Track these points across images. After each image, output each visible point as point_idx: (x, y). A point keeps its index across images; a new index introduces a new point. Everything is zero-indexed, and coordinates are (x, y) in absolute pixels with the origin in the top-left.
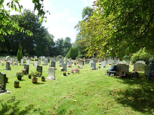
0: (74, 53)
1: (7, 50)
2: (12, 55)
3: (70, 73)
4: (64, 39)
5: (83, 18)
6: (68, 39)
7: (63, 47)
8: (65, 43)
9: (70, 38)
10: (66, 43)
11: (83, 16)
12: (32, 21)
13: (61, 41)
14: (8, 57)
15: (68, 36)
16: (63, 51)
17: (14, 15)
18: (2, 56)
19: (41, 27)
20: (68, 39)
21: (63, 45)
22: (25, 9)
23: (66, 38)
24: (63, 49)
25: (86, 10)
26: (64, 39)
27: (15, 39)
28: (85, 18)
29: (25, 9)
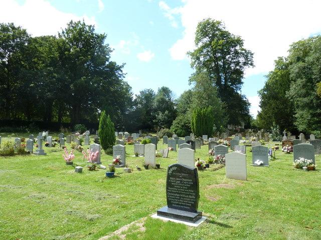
0: (206, 123)
1: (23, 116)
2: (37, 133)
3: (136, 169)
4: (156, 91)
5: (197, 44)
6: (165, 91)
7: (155, 110)
8: (158, 101)
9: (171, 88)
10: (162, 101)
11: (198, 40)
12: (211, 35)
13: (148, 96)
14: (44, 134)
15: (166, 86)
16: (155, 118)
17: (45, 36)
18: (2, 131)
19: (107, 63)
20: (165, 91)
21: (155, 104)
22: (72, 21)
23: (160, 88)
24: (156, 116)
25: (205, 27)
26: (156, 91)
27: (49, 91)
28: (200, 44)
29: (72, 21)
